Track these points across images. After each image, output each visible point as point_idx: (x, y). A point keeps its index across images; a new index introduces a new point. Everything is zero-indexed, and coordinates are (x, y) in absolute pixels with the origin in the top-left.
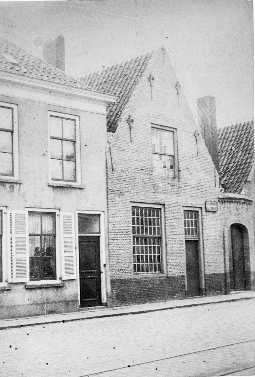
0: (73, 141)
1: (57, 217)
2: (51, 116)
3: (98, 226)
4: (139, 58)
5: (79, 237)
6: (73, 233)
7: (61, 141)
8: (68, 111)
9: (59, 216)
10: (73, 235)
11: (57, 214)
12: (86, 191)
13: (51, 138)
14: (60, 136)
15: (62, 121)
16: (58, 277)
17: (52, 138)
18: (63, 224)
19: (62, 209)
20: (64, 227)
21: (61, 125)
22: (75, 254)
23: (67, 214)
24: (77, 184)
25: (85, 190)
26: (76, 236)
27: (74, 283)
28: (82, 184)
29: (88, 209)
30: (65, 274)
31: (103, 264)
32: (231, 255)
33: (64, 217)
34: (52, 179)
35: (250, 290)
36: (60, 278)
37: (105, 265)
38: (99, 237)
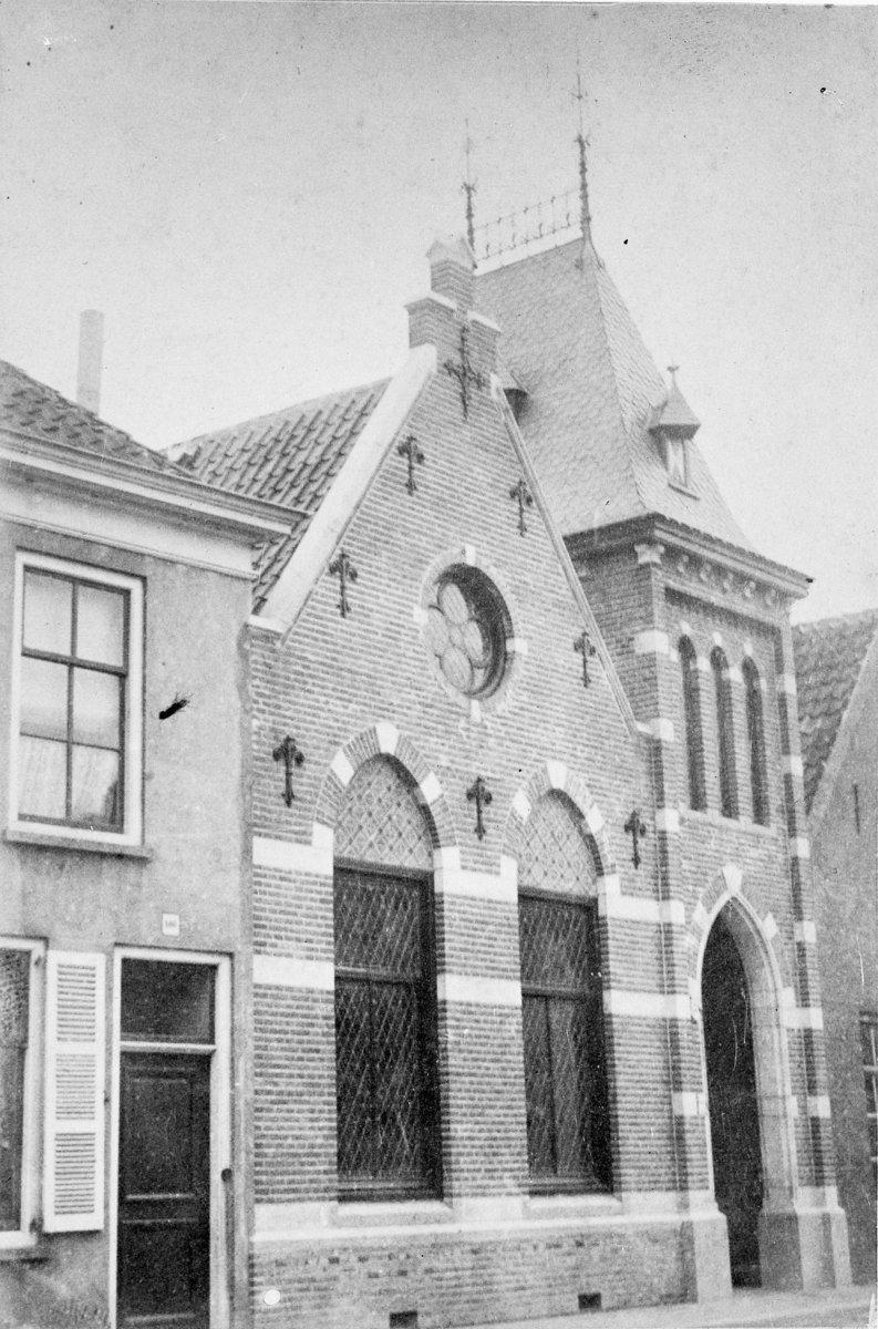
0: (115, 674)
1: (34, 974)
2: (27, 568)
3: (206, 1004)
4: (324, 417)
5: (124, 1054)
6: (100, 1035)
7: (64, 668)
8: (101, 555)
9: (44, 968)
10: (98, 1049)
11: (34, 957)
12: (159, 872)
13: (24, 654)
14: (65, 651)
15: (70, 672)
16: (27, 1216)
17: (31, 656)
18: (55, 1084)
19: (60, 932)
20: (61, 973)
21: (68, 623)
22: (101, 1128)
23: (78, 959)
24: (128, 839)
25: (157, 865)
26: (109, 1051)
27: (93, 1245)
28: (143, 841)
29: (167, 938)
30: (54, 1209)
31: (220, 1170)
32: (239, 537)
33: (63, 969)
34: (22, 817)
35: (778, 1288)
36: (36, 1225)
37: (227, 1175)
38: (205, 1061)
